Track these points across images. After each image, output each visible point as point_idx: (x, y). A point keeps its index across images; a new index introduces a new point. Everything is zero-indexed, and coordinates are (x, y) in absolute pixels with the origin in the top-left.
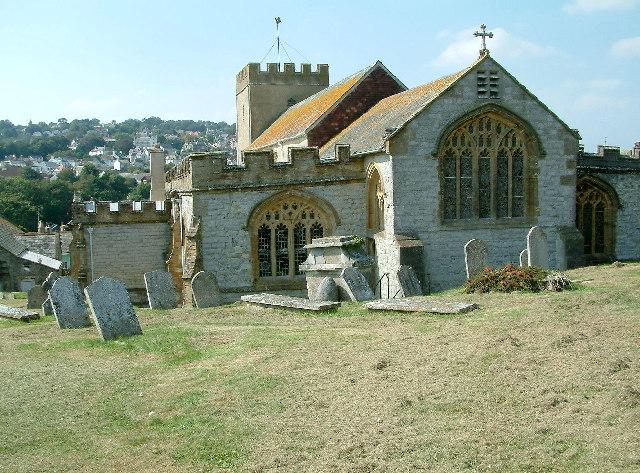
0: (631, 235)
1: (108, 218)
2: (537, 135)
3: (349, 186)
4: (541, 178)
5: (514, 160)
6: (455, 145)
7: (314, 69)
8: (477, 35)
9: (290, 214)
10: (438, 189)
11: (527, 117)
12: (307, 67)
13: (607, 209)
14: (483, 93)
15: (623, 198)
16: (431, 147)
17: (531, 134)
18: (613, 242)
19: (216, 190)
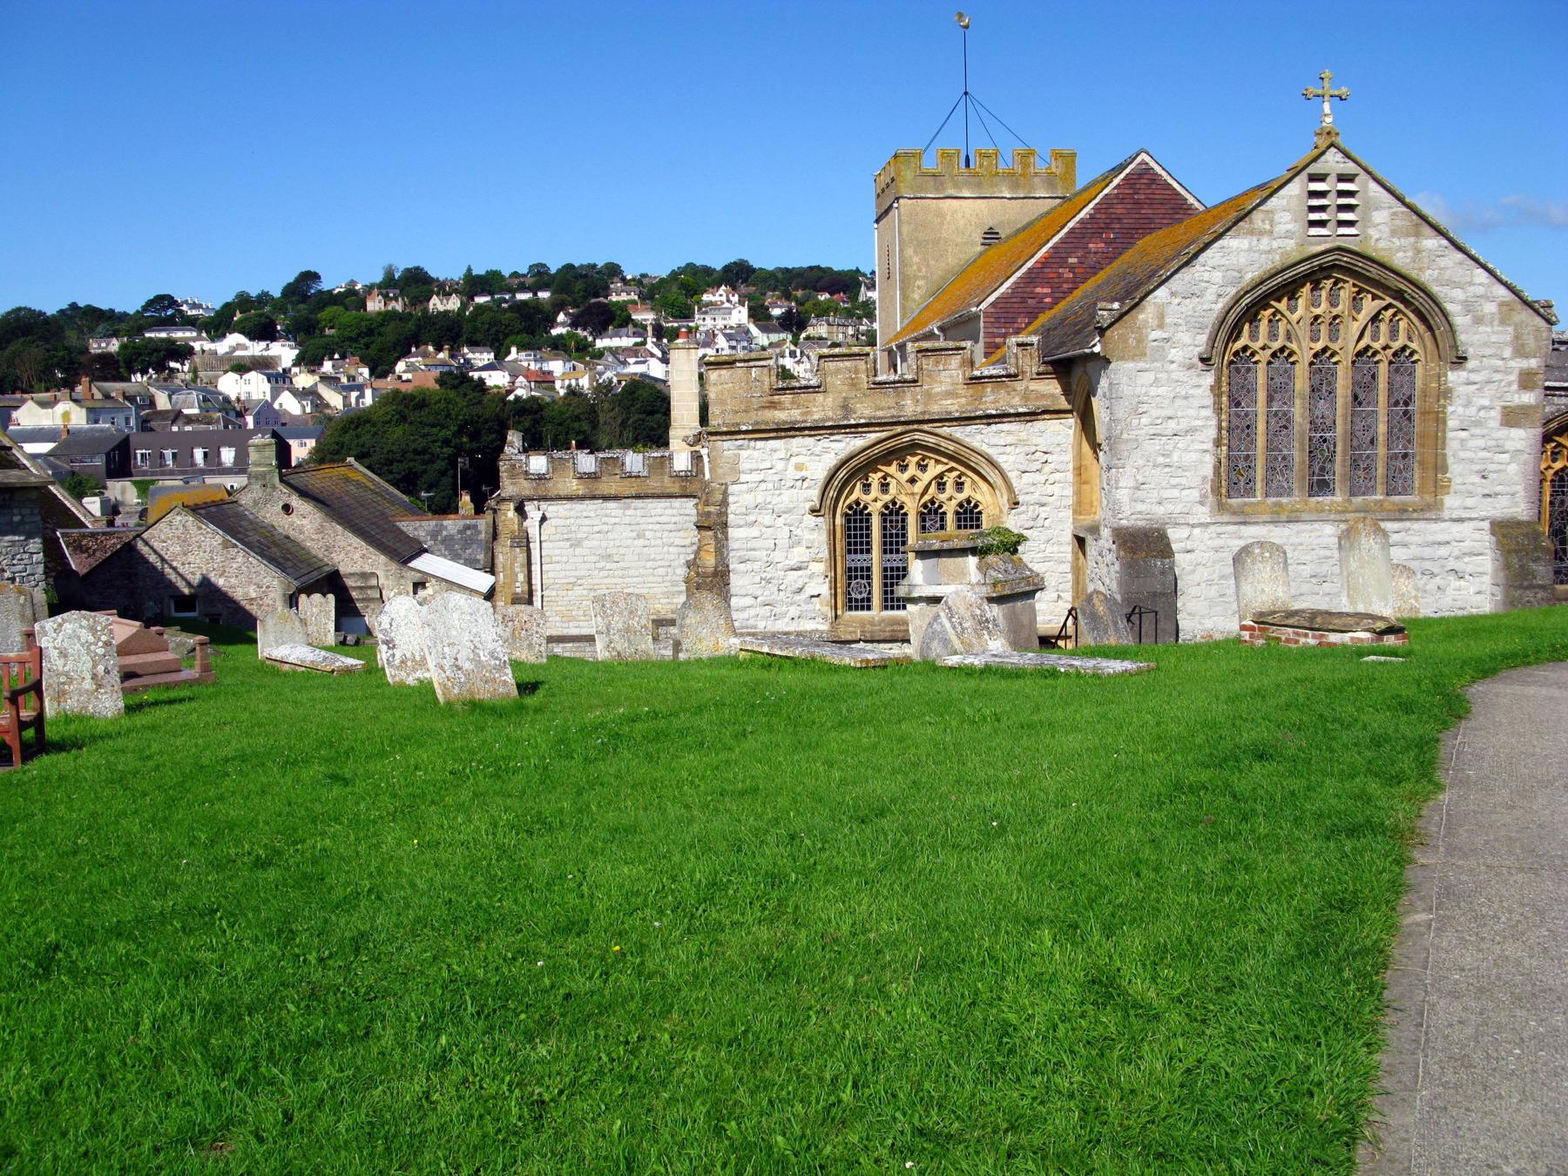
1: (574, 486)
3: (1038, 425)
4: (1455, 413)
9: (912, 481)
11: (1426, 277)
14: (1322, 224)
16: (1199, 342)
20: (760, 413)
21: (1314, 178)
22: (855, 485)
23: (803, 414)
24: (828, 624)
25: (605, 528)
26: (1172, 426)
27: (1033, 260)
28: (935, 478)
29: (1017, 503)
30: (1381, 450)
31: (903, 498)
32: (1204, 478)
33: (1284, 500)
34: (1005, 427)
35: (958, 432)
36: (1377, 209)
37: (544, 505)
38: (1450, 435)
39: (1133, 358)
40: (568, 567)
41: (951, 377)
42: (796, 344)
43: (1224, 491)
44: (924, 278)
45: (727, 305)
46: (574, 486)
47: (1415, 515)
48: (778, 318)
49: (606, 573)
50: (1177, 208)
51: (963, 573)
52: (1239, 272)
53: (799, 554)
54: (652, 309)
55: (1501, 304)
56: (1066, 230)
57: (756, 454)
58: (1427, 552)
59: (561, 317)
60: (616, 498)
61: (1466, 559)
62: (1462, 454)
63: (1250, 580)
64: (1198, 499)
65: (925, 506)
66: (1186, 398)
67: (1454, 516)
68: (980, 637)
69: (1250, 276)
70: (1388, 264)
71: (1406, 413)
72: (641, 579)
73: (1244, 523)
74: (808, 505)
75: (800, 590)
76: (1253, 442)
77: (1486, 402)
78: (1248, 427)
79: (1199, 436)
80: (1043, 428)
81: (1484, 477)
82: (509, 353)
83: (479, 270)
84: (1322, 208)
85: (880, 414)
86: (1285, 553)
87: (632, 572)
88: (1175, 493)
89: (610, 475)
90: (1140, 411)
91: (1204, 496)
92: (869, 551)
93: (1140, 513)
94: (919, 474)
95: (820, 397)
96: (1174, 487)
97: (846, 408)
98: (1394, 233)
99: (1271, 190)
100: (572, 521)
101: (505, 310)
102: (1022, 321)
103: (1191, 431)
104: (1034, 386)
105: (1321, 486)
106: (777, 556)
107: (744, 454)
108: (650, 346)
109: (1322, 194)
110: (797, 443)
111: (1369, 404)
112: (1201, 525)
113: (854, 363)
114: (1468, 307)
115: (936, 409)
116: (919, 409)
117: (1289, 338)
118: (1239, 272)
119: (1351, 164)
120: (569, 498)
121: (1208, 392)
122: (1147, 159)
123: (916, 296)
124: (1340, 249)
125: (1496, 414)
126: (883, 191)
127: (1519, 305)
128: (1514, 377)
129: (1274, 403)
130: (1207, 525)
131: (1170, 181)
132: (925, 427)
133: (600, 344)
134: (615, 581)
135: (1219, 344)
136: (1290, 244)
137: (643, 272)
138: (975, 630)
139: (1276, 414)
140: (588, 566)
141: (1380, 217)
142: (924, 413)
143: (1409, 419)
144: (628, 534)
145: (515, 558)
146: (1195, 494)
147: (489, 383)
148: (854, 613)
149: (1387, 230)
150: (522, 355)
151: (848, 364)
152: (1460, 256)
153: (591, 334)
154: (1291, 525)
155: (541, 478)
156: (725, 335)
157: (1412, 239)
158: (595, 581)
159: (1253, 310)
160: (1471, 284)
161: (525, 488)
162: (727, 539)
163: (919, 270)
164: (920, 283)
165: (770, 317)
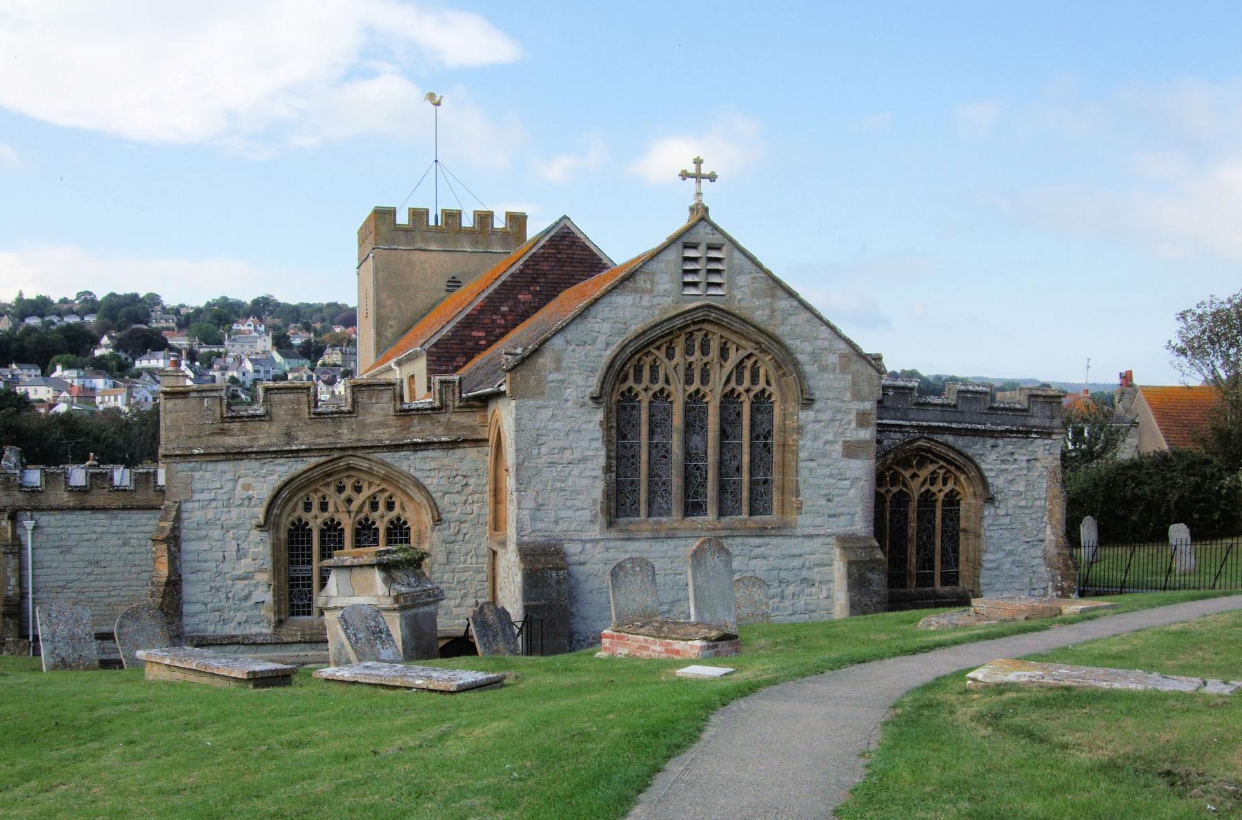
0: (1010, 553)
1: (64, 498)
2: (796, 363)
3: (459, 453)
4: (806, 446)
5: (754, 410)
6: (638, 379)
7: (499, 223)
8: (712, 178)
10: (602, 461)
11: (781, 331)
12: (484, 218)
13: (968, 504)
14: (695, 284)
15: (997, 482)
17: (786, 360)
18: (977, 564)
19: (211, 456)
20: (211, 438)
21: (687, 246)
22: (296, 504)
23: (250, 440)
24: (272, 627)
25: (94, 536)
26: (568, 455)
27: (471, 308)
28: (369, 497)
29: (440, 520)
30: (746, 477)
32: (595, 501)
33: (664, 519)
34: (430, 454)
35: (388, 457)
36: (739, 274)
37: (36, 515)
38: (802, 464)
39: (533, 396)
42: (312, 370)
43: (613, 511)
44: (395, 318)
45: (255, 334)
46: (64, 498)
47: (773, 532)
48: (298, 347)
49: (94, 577)
50: (590, 262)
51: (372, 586)
52: (625, 324)
53: (246, 564)
54: (187, 335)
55: (842, 356)
56: (499, 282)
57: (207, 475)
58: (784, 563)
59: (105, 340)
60: (104, 509)
61: (816, 570)
62: (811, 481)
63: (622, 591)
64: (589, 519)
65: (360, 523)
66: (579, 431)
67: (805, 533)
68: (373, 646)
69: (635, 327)
70: (749, 321)
71: (765, 445)
72: (126, 583)
73: (629, 539)
74: (254, 522)
75: (247, 598)
76: (637, 469)
77: (831, 437)
78: (633, 456)
80: (463, 456)
81: (829, 500)
82: (55, 370)
83: (30, 295)
84: (695, 272)
85: (320, 441)
86: (653, 567)
87: (117, 577)
88: (569, 513)
89: (99, 488)
90: (540, 442)
91: (595, 516)
92: (310, 562)
93: (539, 530)
94: (354, 495)
95: (266, 426)
96: (569, 508)
97: (289, 436)
98: (753, 294)
100: (63, 529)
101: (53, 332)
102: (460, 360)
103: (584, 460)
104: (455, 418)
105: (693, 507)
106: (226, 567)
107: (197, 475)
109: (695, 260)
110: (245, 466)
111: (735, 438)
112: (591, 541)
113: (296, 396)
114: (814, 356)
115: (369, 437)
116: (354, 437)
117: (667, 381)
118: (625, 324)
119: (718, 236)
120: (60, 509)
121: (598, 427)
123: (389, 334)
124: (708, 306)
125: (838, 447)
128: (852, 417)
129: (656, 436)
130: (596, 541)
132: (360, 453)
133: (138, 364)
134: (101, 584)
135: (608, 387)
136: (667, 301)
137: (182, 303)
138: (369, 640)
139: (657, 446)
140: (78, 571)
141: (742, 280)
142: (359, 440)
143: (769, 451)
144: (114, 541)
145: (8, 563)
146: (587, 515)
147: (32, 396)
149: (748, 291)
150: (66, 373)
151: (291, 396)
152: (808, 315)
153: (131, 355)
154: (669, 541)
155: (34, 491)
156: (251, 360)
158: (83, 585)
159: (637, 357)
160: (816, 338)
162: (179, 551)
163: (392, 312)
164: (392, 323)
165: (291, 346)
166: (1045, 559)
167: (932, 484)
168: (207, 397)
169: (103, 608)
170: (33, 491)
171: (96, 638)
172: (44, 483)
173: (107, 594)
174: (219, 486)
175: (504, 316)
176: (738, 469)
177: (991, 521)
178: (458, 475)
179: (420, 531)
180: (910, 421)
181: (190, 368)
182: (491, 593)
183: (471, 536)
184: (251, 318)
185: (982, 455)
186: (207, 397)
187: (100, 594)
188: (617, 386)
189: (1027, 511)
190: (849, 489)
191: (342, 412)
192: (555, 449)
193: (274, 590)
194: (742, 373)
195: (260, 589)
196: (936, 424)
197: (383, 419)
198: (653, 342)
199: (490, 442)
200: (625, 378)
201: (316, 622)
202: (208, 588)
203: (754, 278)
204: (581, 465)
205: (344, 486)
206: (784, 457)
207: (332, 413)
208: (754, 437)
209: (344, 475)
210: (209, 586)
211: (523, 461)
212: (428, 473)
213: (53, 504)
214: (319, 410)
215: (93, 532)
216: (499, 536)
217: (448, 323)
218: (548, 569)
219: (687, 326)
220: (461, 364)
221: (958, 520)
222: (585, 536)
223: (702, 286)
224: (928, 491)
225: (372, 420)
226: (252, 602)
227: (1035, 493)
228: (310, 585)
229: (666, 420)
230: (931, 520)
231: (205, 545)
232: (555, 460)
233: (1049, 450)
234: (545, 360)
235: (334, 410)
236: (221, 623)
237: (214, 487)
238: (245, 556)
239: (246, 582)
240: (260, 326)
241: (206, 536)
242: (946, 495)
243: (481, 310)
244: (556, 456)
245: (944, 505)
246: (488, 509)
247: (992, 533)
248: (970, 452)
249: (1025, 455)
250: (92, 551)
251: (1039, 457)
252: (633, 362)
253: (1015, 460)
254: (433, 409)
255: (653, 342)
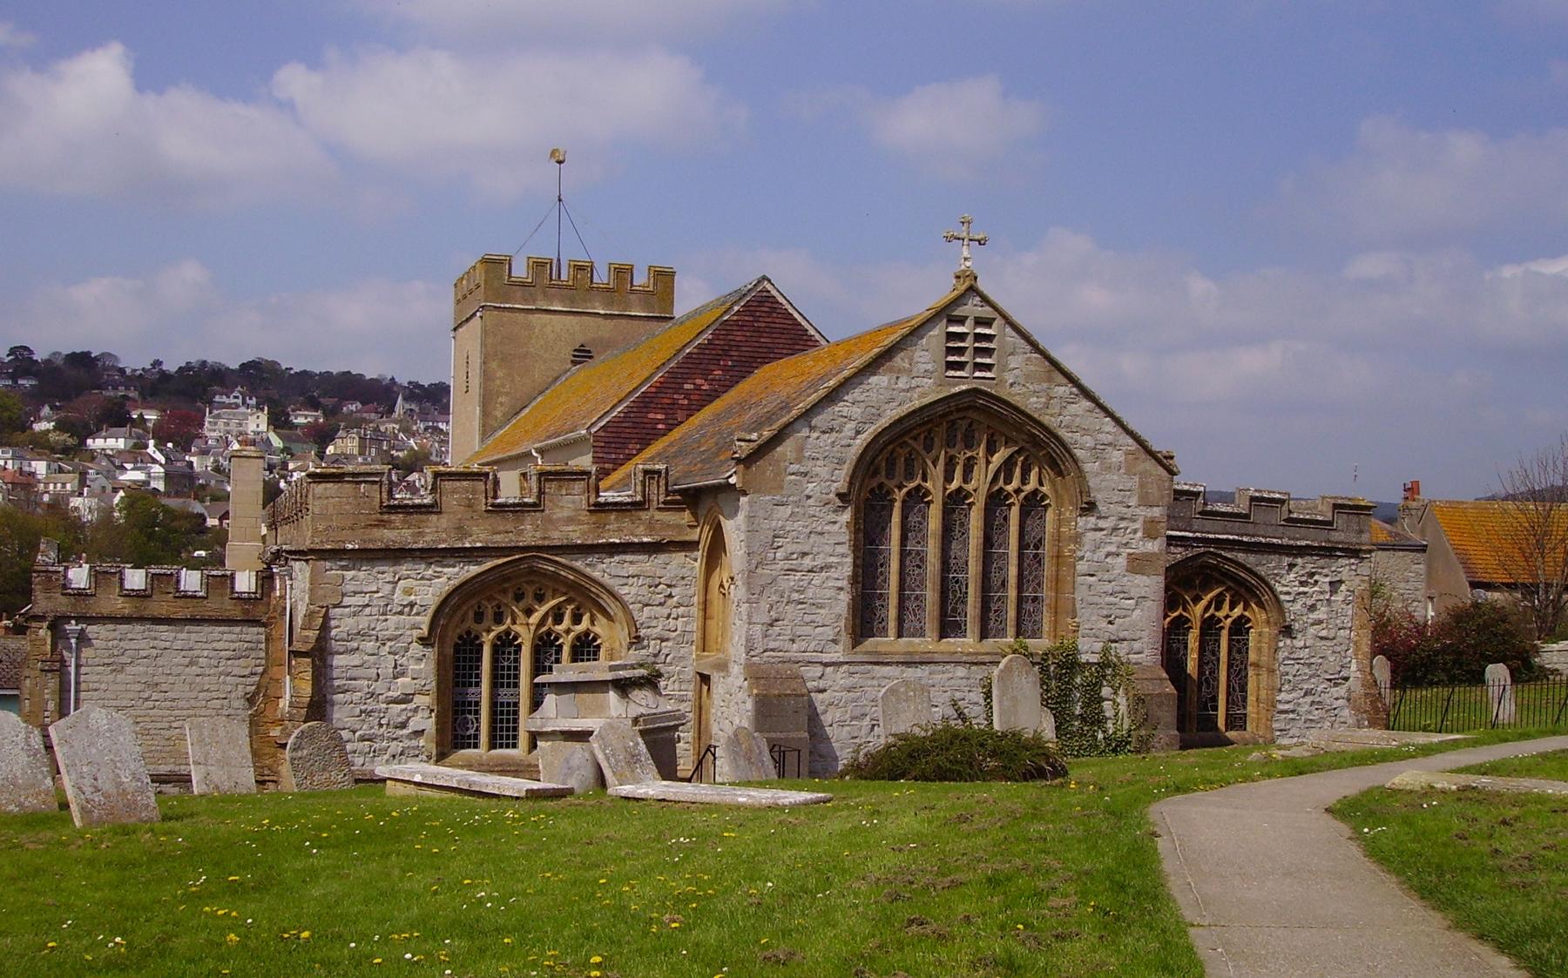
1: (121, 606)
3: (662, 558)
10: (847, 570)
20: (368, 531)
22: (466, 613)
23: (413, 535)
25: (154, 652)
30: (1012, 593)
31: (517, 628)
33: (917, 640)
38: (1080, 579)
40: (108, 695)
41: (574, 502)
44: (507, 394)
65: (541, 638)
71: (1036, 556)
74: (416, 633)
75: (403, 725)
79: (833, 573)
81: (1110, 623)
85: (498, 538)
87: (181, 704)
88: (808, 630)
95: (434, 518)
97: (461, 531)
99: (917, 332)
104: (659, 516)
105: (949, 626)
106: (379, 687)
108: (151, 449)
113: (471, 483)
115: (557, 537)
119: (988, 308)
122: (769, 287)
123: (498, 414)
125: (1121, 561)
126: (465, 297)
127: (1143, 456)
131: (791, 310)
134: (161, 713)
137: (54, 350)
143: (1039, 562)
148: (498, 751)
152: (1087, 404)
155: (80, 594)
157: (1045, 385)
158: (139, 712)
159: (890, 448)
160: (1100, 431)
161: (61, 604)
163: (503, 386)
166: (1349, 700)
167: (1218, 608)
168: (365, 482)
169: (161, 744)
170: (80, 595)
171: (153, 781)
172: (93, 585)
173: (167, 725)
174: (375, 589)
175: (687, 395)
176: (1004, 584)
177: (1286, 654)
178: (660, 583)
179: (612, 649)
180: (1194, 532)
181: (161, 451)
182: (697, 726)
183: (674, 659)
184: (239, 388)
185: (1277, 575)
186: (365, 482)
187: (159, 725)
188: (866, 481)
189: (1328, 643)
190: (1133, 610)
191: (526, 505)
192: (793, 554)
193: (437, 717)
194: (1011, 470)
195: (420, 714)
196: (1225, 537)
197: (574, 513)
198: (911, 430)
199: (701, 546)
200: (876, 472)
201: (485, 757)
202: (357, 711)
203: (1028, 359)
204: (823, 574)
205: (523, 594)
206: (1057, 571)
207: (514, 505)
208: (1022, 546)
209: (524, 579)
210: (358, 710)
211: (756, 567)
212: (625, 581)
213: (103, 611)
214: (498, 501)
215: (153, 648)
216: (712, 656)
217: (620, 401)
218: (786, 695)
219: (951, 413)
220: (634, 452)
221: (1247, 653)
222: (826, 658)
223: (968, 367)
224: (1213, 616)
225: (560, 515)
226: (410, 731)
227: (1338, 621)
228: (516, 713)
229: (920, 523)
230: (1215, 653)
231: (355, 659)
232: (793, 567)
233: (1356, 571)
234: (786, 449)
235: (517, 501)
236: (371, 755)
237: (370, 590)
238: (403, 674)
239: (404, 706)
240: (250, 399)
241: (358, 649)
242: (1234, 622)
243: (661, 387)
244: (794, 562)
245: (1230, 634)
246: (695, 626)
247: (1287, 669)
248: (1261, 570)
249: (1327, 576)
250: (150, 670)
251: (1344, 579)
252: (885, 454)
253: (1316, 582)
254: (633, 504)
255: (911, 430)
